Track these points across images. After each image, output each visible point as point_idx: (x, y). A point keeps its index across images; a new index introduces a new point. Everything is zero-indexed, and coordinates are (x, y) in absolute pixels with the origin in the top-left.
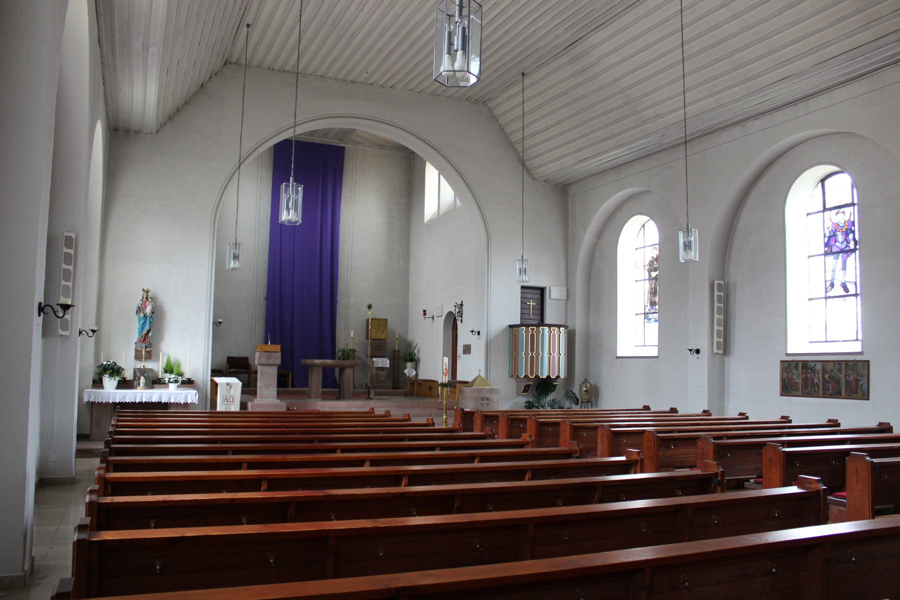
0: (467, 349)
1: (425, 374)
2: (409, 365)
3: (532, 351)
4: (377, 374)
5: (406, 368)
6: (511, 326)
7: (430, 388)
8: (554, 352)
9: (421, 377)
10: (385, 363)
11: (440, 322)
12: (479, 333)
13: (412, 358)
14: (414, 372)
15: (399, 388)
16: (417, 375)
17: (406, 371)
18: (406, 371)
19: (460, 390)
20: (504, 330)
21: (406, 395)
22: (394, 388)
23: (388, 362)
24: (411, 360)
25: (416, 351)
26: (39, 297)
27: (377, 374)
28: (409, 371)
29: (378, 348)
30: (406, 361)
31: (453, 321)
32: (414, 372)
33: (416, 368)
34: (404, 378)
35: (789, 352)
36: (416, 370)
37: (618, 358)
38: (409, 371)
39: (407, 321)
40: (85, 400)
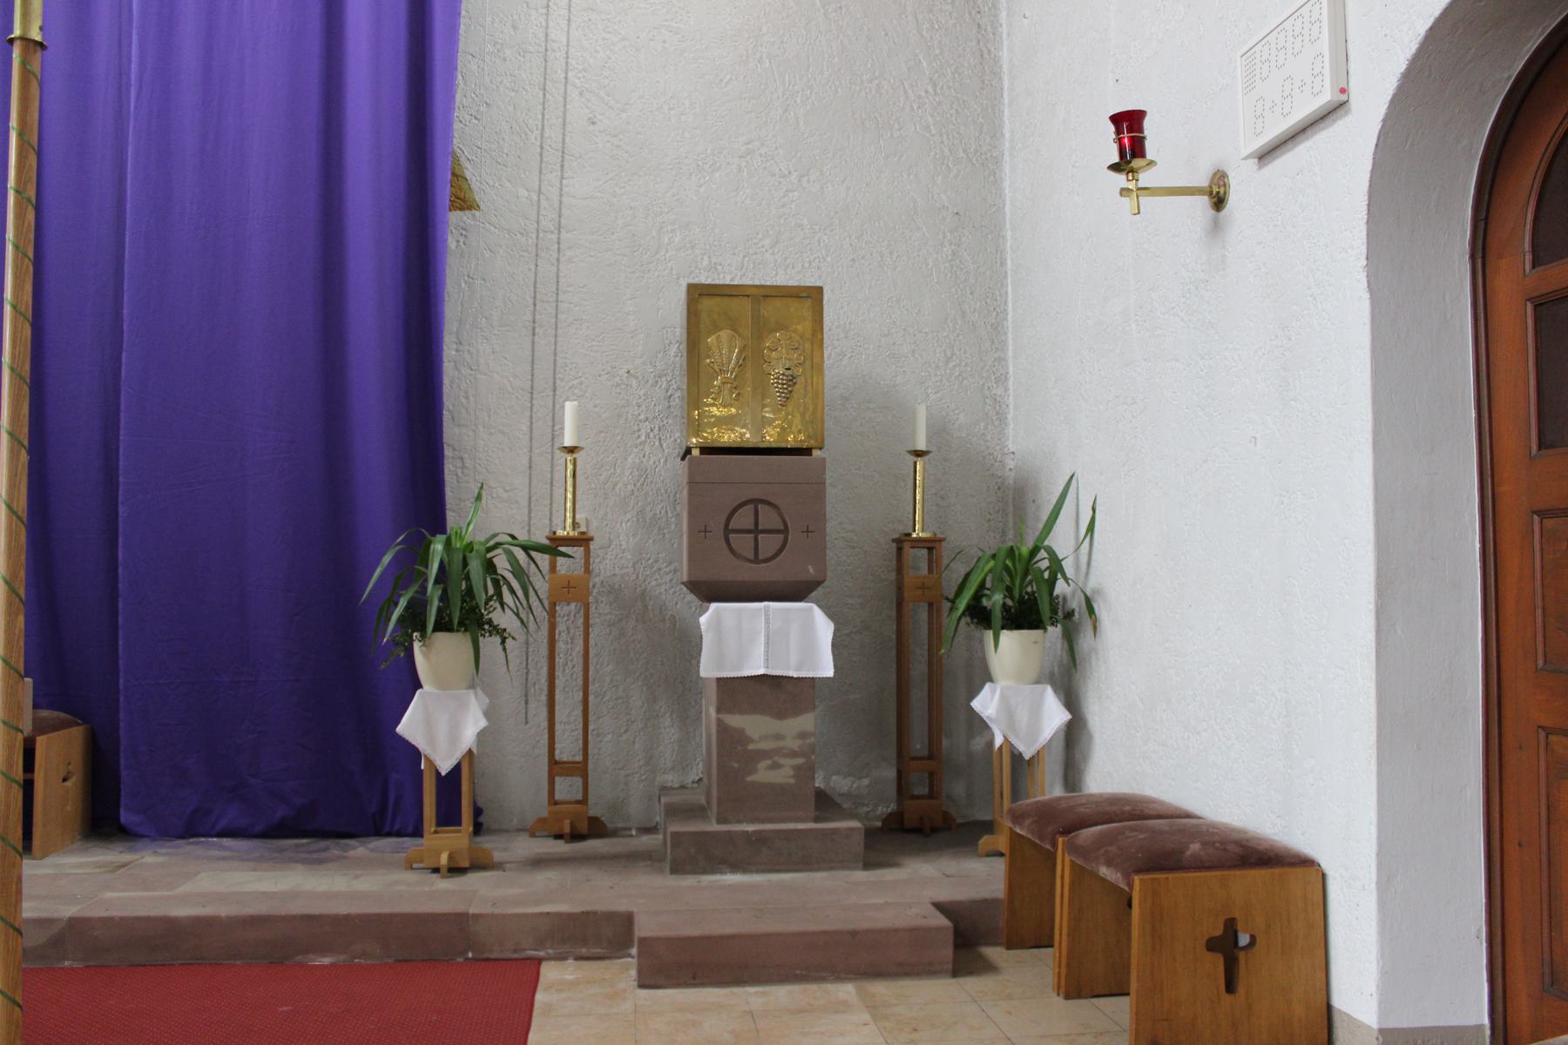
2: (1010, 650)
4: (730, 741)
5: (980, 675)
9: (1109, 774)
10: (789, 639)
14: (1055, 715)
16: (1074, 735)
17: (986, 703)
18: (986, 703)
23: (824, 629)
24: (1025, 616)
25: (1062, 540)
27: (730, 741)
29: (751, 520)
30: (979, 615)
32: (1055, 715)
33: (1067, 680)
36: (1071, 700)
38: (1011, 698)
39: (997, 328)
40: (1055, 632)
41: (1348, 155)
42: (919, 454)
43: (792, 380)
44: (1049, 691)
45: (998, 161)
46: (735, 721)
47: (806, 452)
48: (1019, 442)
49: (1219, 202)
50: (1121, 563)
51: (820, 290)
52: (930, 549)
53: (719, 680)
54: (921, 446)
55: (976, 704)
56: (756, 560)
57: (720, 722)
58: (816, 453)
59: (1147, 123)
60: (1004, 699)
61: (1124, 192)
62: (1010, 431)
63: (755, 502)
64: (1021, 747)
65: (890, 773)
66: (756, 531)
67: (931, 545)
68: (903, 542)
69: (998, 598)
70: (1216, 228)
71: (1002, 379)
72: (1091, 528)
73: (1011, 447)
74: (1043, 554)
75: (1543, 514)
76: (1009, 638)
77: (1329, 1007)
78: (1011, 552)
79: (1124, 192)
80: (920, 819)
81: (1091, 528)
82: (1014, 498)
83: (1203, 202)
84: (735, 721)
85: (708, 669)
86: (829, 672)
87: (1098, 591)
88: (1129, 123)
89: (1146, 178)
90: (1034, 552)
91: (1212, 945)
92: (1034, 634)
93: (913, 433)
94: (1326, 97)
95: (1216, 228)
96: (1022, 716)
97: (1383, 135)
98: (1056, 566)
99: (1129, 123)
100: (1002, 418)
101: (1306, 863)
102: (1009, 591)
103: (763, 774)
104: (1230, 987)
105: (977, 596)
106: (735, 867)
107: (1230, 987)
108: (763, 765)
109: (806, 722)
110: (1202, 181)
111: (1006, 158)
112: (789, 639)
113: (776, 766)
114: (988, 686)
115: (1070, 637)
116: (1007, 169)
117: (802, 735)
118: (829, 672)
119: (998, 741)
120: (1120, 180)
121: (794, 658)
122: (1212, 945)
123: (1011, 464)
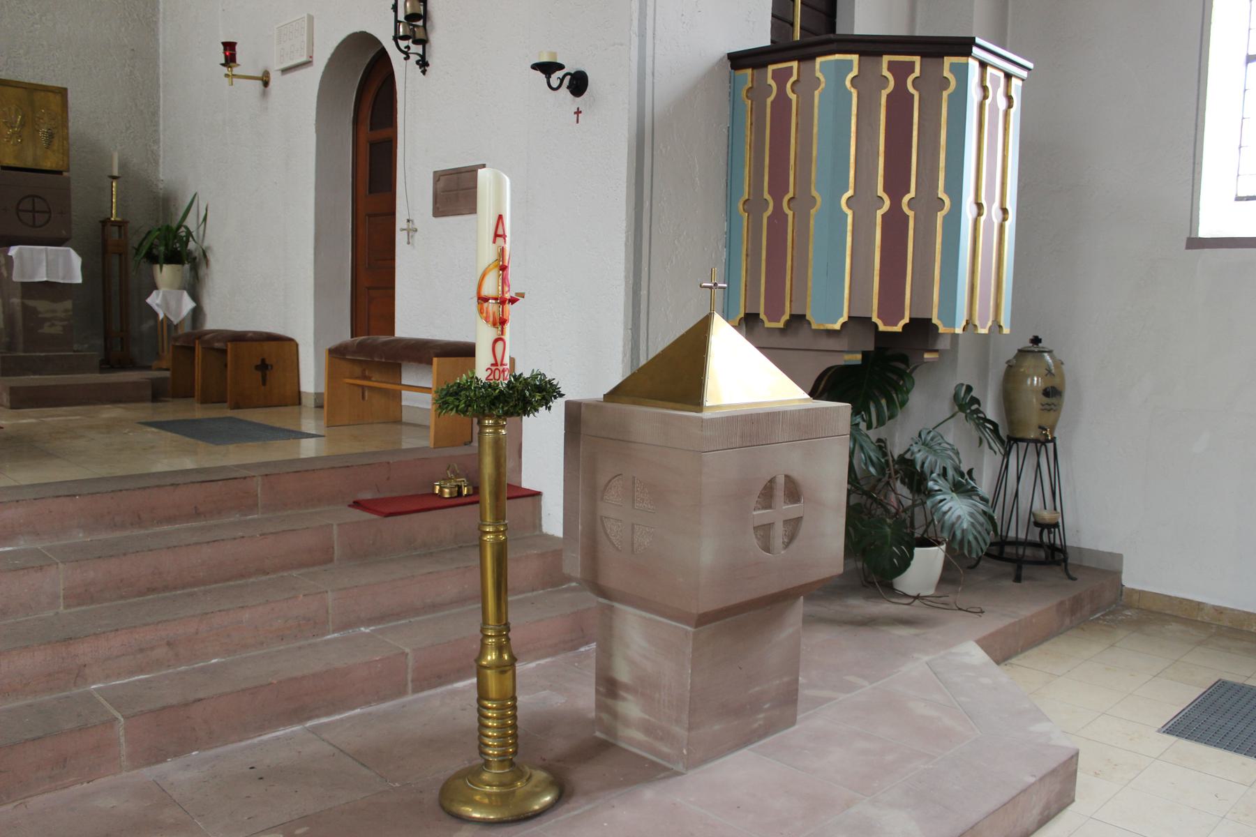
0: (455, 193)
1: (233, 305)
2: (166, 274)
3: (896, 185)
4: (28, 312)
5: (154, 287)
6: (738, 60)
7: (263, 367)
8: (991, 201)
9: (215, 321)
10: (63, 265)
11: (301, 97)
12: (578, 84)
13: (176, 247)
14: (188, 304)
15: (126, 363)
16: (197, 313)
17: (154, 300)
18: (154, 300)
19: (498, 444)
20: (711, 73)
21: (157, 393)
22: (110, 363)
23: (77, 261)
24: (175, 257)
25: (191, 222)
26: (507, 327)
27: (28, 312)
28: (167, 299)
30: (153, 259)
31: (367, 90)
32: (188, 304)
33: (194, 288)
34: (147, 325)
35: (1204, 232)
36: (195, 296)
37: (1196, 243)
38: (167, 299)
39: (155, 113)
40: (187, 266)
41: (312, 78)
42: (114, 178)
43: (51, 136)
44: (185, 294)
45: (156, 23)
46: (31, 303)
47: (60, 173)
48: (165, 175)
49: (266, 84)
50: (223, 235)
51: (66, 90)
52: (120, 227)
53: (23, 284)
54: (116, 173)
55: (149, 301)
56: (34, 226)
57: (25, 308)
58: (65, 174)
59: (237, 48)
60: (164, 297)
61: (227, 75)
62: (161, 169)
63: (34, 196)
64: (172, 318)
65: (100, 342)
66: (34, 211)
67: (121, 225)
68: (105, 222)
69: (162, 248)
70: (264, 94)
71: (157, 142)
72: (205, 219)
73: (162, 177)
74: (183, 229)
75: (370, 216)
76: (167, 268)
77: (299, 392)
78: (168, 227)
79: (227, 75)
80: (116, 357)
81: (205, 219)
82: (163, 203)
83: (259, 83)
84: (31, 303)
85: (16, 278)
86: (80, 281)
87: (209, 248)
88: (229, 47)
89: (236, 71)
90: (179, 227)
91: (257, 367)
92: (179, 266)
93: (111, 165)
94: (304, 59)
95: (264, 94)
96: (173, 304)
97: (324, 73)
98: (189, 233)
99: (229, 47)
100: (157, 163)
101: (291, 340)
102: (166, 245)
103: (47, 329)
104: (264, 383)
105: (151, 248)
106: (35, 373)
107: (264, 383)
108: (47, 324)
109: (68, 304)
110: (260, 75)
111: (161, 22)
112: (63, 265)
113: (53, 325)
114: (155, 293)
115: (195, 268)
116: (161, 29)
117: (66, 311)
118: (80, 281)
119: (161, 316)
120: (225, 70)
121: (61, 274)
122: (257, 367)
123: (161, 186)
